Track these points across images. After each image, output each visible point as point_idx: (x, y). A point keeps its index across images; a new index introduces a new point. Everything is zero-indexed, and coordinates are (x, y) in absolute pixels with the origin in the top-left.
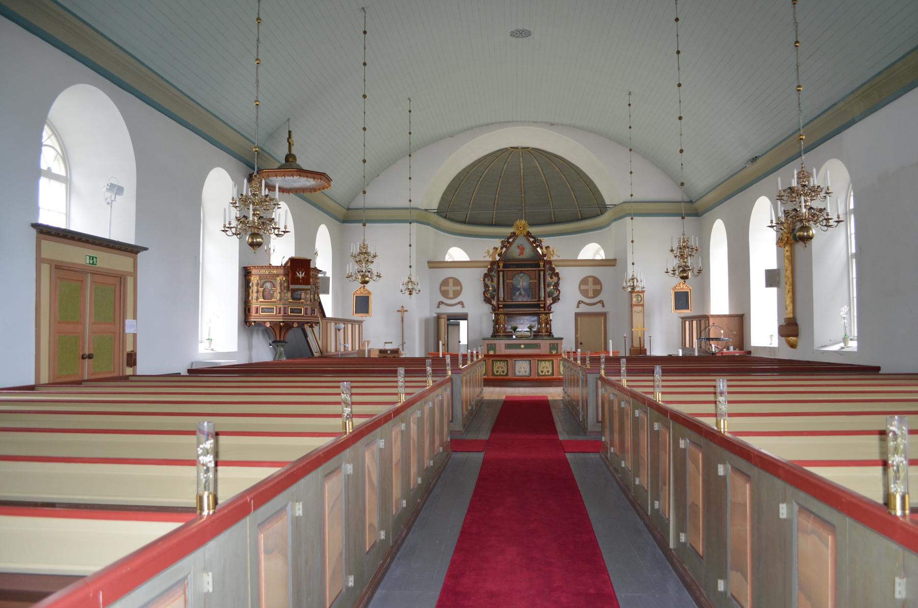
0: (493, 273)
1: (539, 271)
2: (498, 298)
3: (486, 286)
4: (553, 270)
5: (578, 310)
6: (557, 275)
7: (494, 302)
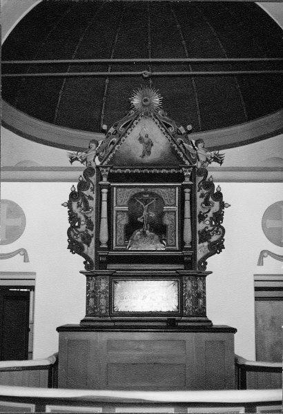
0: (87, 193)
2: (98, 242)
3: (73, 218)
4: (209, 185)
5: (261, 270)
6: (219, 196)
7: (90, 250)
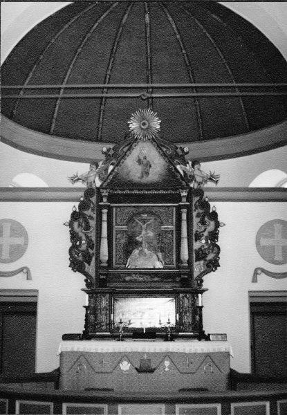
0: (88, 212)
1: (179, 209)
3: (74, 236)
6: (214, 216)
